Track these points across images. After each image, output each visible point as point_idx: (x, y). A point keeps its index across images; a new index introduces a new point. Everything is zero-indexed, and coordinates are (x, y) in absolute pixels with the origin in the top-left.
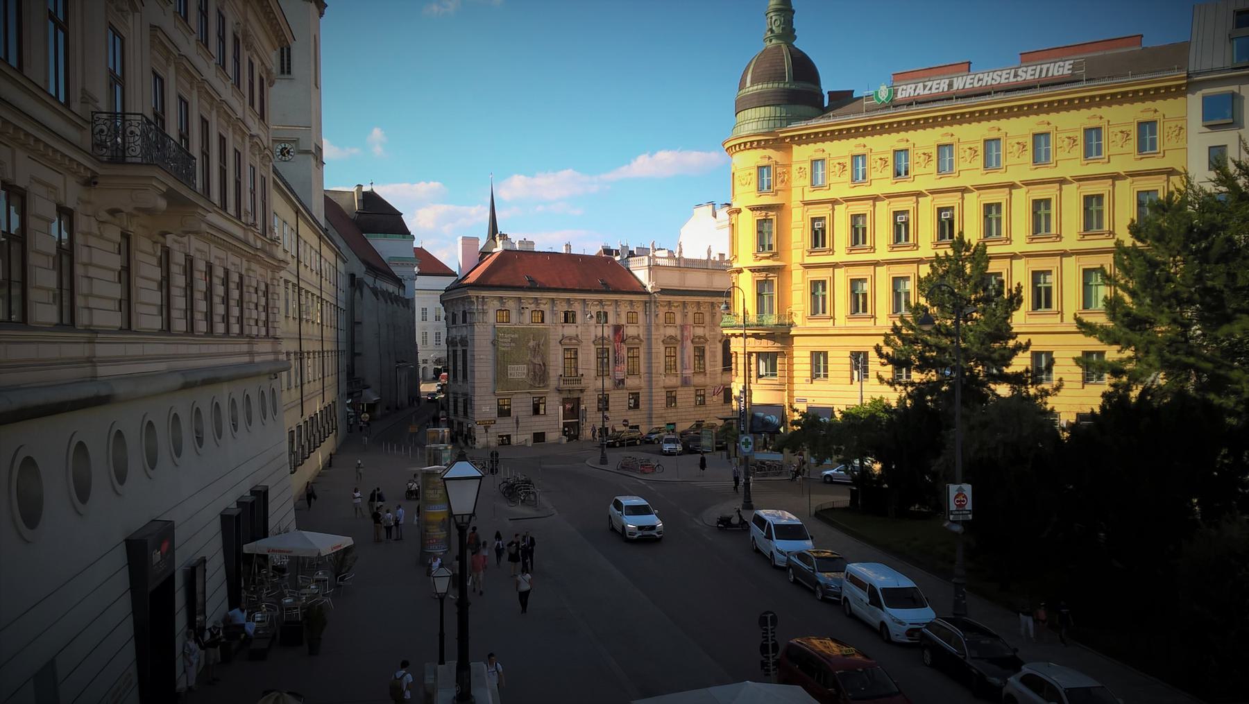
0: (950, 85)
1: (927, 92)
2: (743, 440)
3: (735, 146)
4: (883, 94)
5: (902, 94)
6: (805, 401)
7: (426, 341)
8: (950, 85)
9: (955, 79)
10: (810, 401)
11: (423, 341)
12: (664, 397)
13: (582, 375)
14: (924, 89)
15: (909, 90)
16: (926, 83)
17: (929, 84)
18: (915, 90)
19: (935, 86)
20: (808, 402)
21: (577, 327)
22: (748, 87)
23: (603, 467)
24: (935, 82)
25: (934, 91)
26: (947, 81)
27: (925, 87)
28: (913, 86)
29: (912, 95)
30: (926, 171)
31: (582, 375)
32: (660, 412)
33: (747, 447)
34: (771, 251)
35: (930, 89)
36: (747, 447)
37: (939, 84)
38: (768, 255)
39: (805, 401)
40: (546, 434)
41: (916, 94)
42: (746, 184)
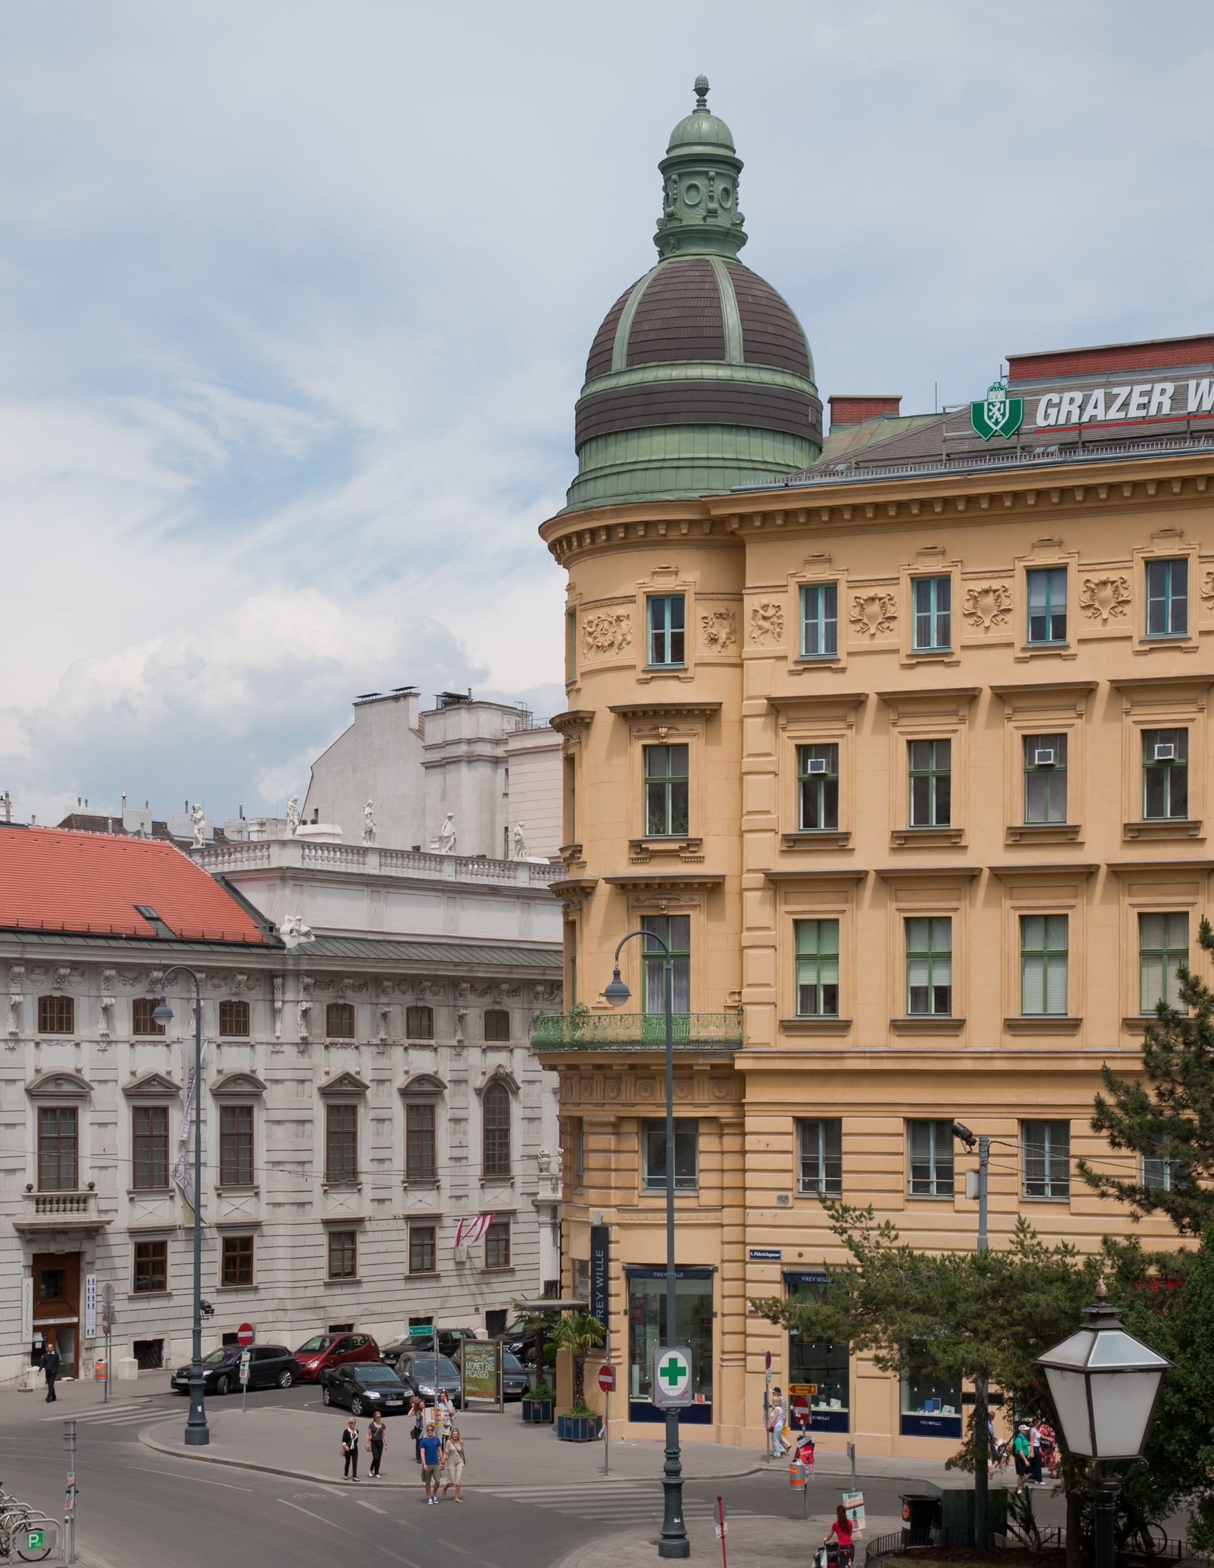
0: (1179, 398)
1: (1113, 414)
2: (664, 1363)
3: (580, 535)
4: (997, 414)
5: (1046, 416)
6: (773, 1256)
7: (678, 641)
8: (1179, 398)
9: (1192, 384)
10: (789, 1255)
11: (659, 640)
12: (171, 1271)
13: (91, 1186)
14: (1107, 408)
15: (1065, 407)
16: (1115, 391)
17: (1123, 391)
18: (1082, 408)
19: (1136, 400)
20: (784, 1259)
21: (77, 1045)
22: (619, 373)
23: (194, 1450)
24: (1138, 389)
25: (1133, 412)
26: (1170, 387)
27: (1110, 400)
28: (1078, 396)
29: (1074, 419)
30: (1113, 629)
31: (91, 1186)
32: (310, 1292)
33: (673, 1382)
34: (680, 836)
35: (1125, 405)
36: (673, 1382)
37: (1149, 394)
38: (675, 846)
39: (773, 1256)
40: (165, 1344)
41: (1085, 418)
42: (612, 644)
